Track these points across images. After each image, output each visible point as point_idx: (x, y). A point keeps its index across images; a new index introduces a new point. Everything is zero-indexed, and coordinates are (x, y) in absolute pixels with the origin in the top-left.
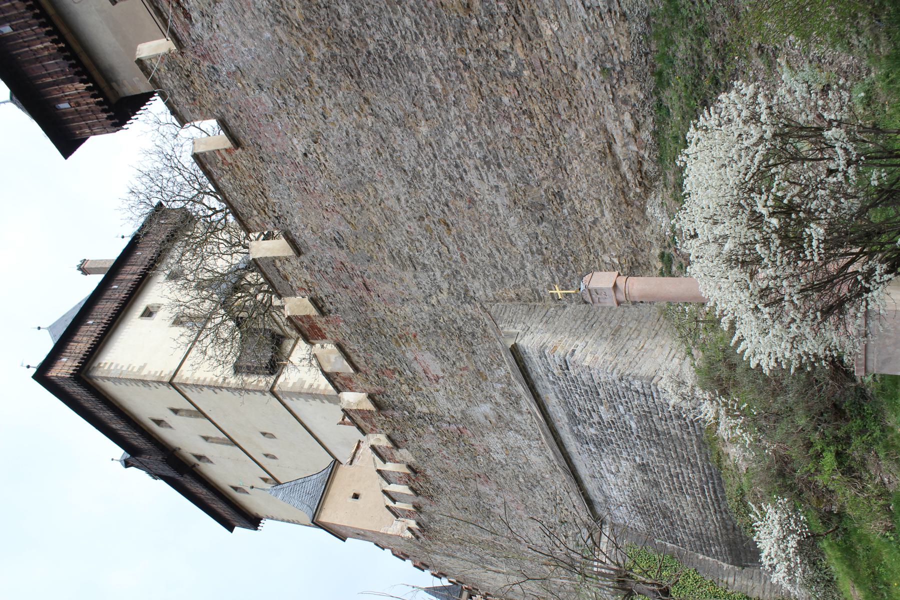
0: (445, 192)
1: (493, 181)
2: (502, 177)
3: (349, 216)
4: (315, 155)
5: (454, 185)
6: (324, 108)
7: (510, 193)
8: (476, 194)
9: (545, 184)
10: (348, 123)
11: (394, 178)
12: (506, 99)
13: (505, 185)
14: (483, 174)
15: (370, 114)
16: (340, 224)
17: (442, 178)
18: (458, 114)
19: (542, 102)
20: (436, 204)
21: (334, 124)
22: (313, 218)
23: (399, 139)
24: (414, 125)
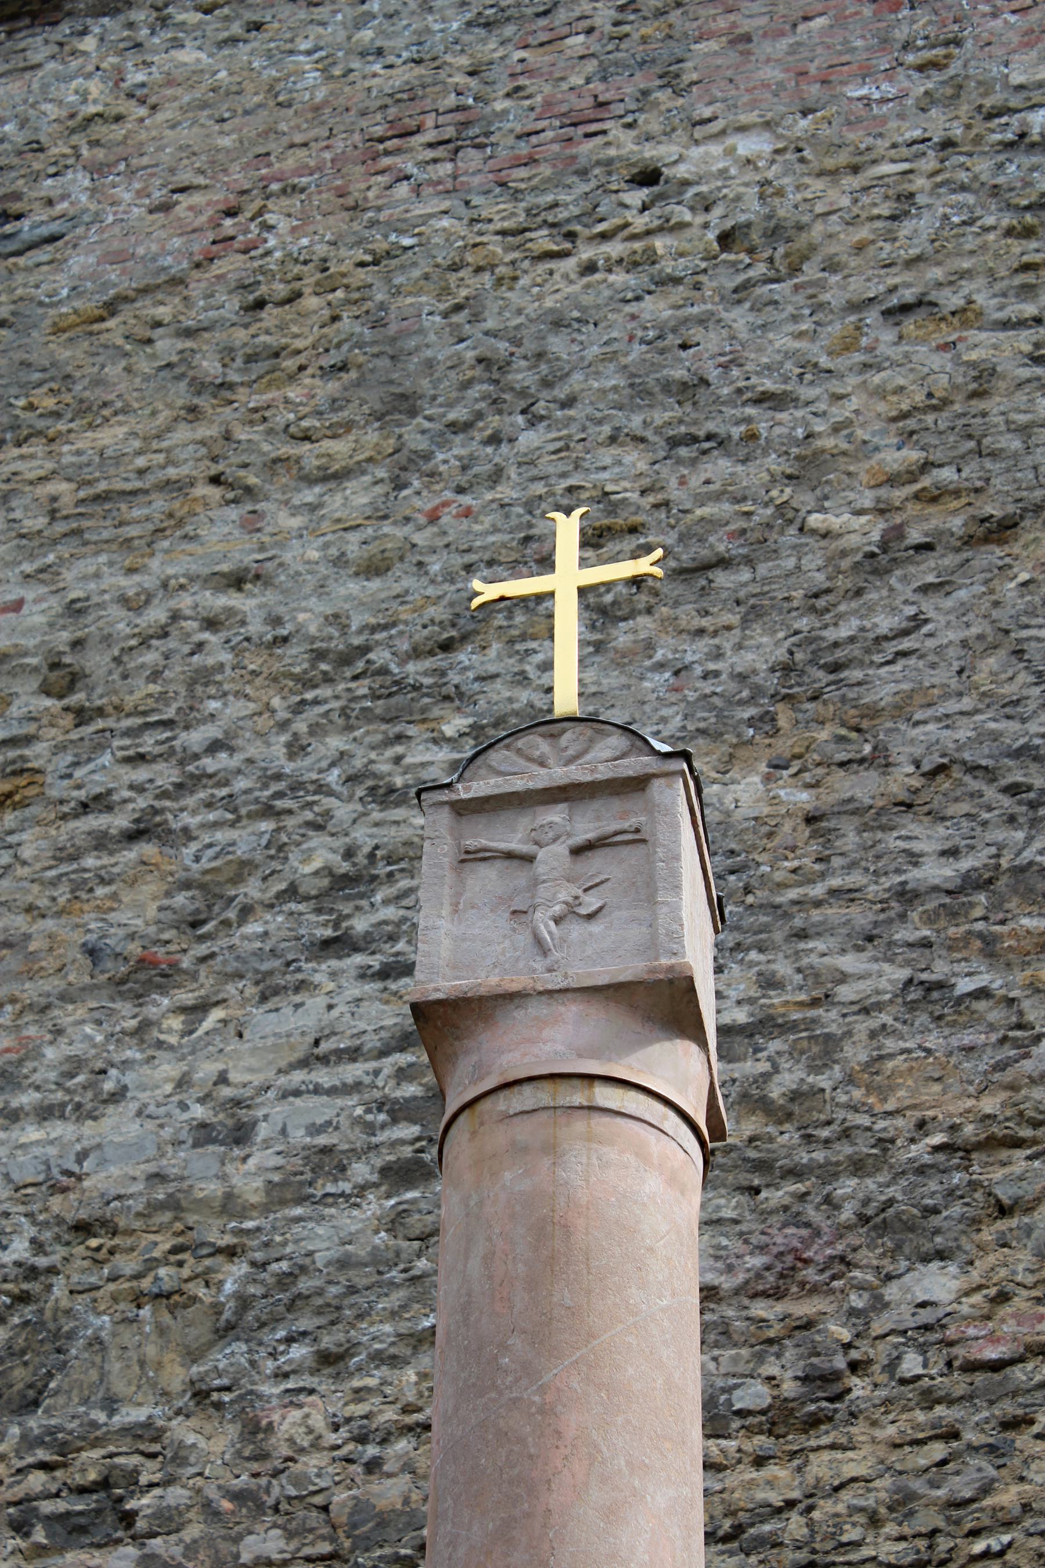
0: (247, 839)
1: (288, 1123)
3: (163, 312)
5: (292, 892)
6: (966, 315)
7: (173, 1204)
8: (201, 1008)
9: (211, 1442)
12: (939, 1283)
15: (897, 533)
16: (118, 258)
17: (363, 836)
18: (846, 992)
19: (903, 1503)
20: (166, 775)
21: (848, 345)
22: (186, 134)
23: (694, 652)
24: (784, 746)
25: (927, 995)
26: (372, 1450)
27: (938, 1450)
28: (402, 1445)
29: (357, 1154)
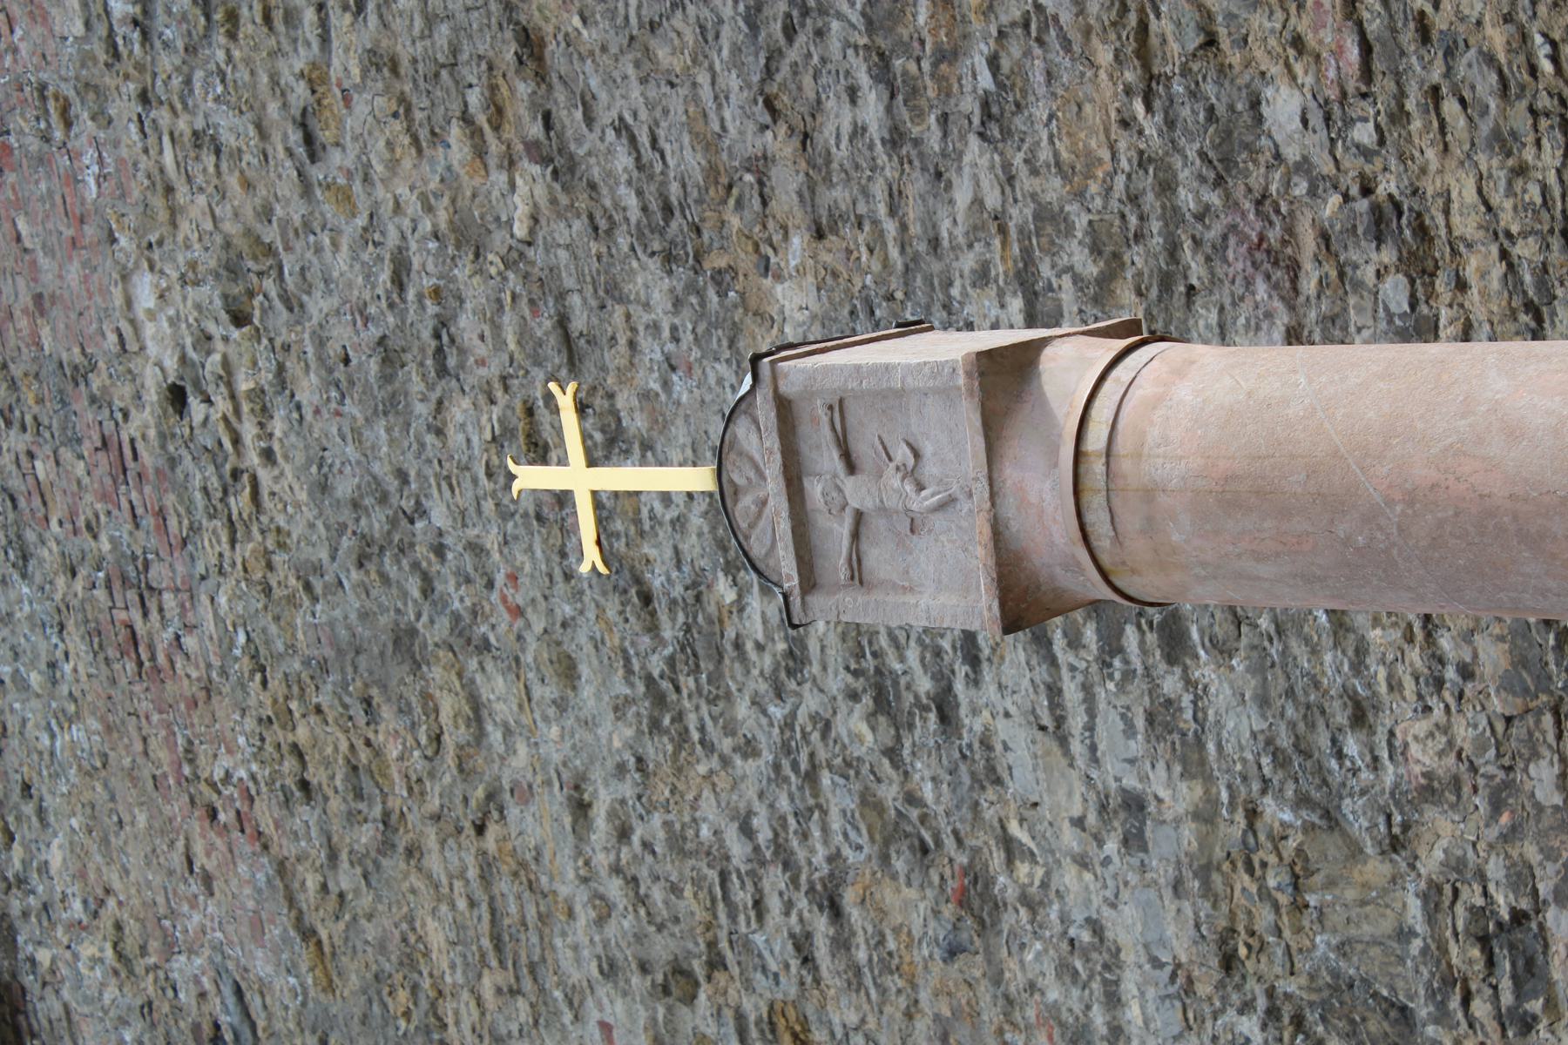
0: (839, 798)
1: (1124, 757)
2: (1175, 732)
3: (312, 882)
4: (222, 405)
5: (892, 753)
6: (315, 78)
7: (1204, 872)
8: (1009, 845)
9: (1443, 835)
10: (413, 205)
11: (580, 642)
12: (1284, 107)
13: (1187, 795)
14: (1071, 692)
16: (258, 927)
17: (837, 682)
18: (992, 199)
19: (1503, 142)
20: (775, 879)
21: (345, 197)
22: (134, 859)
23: (651, 351)
24: (746, 261)
25: (995, 118)
26: (1450, 673)
27: (1450, 107)
28: (1445, 643)
29: (1154, 689)
